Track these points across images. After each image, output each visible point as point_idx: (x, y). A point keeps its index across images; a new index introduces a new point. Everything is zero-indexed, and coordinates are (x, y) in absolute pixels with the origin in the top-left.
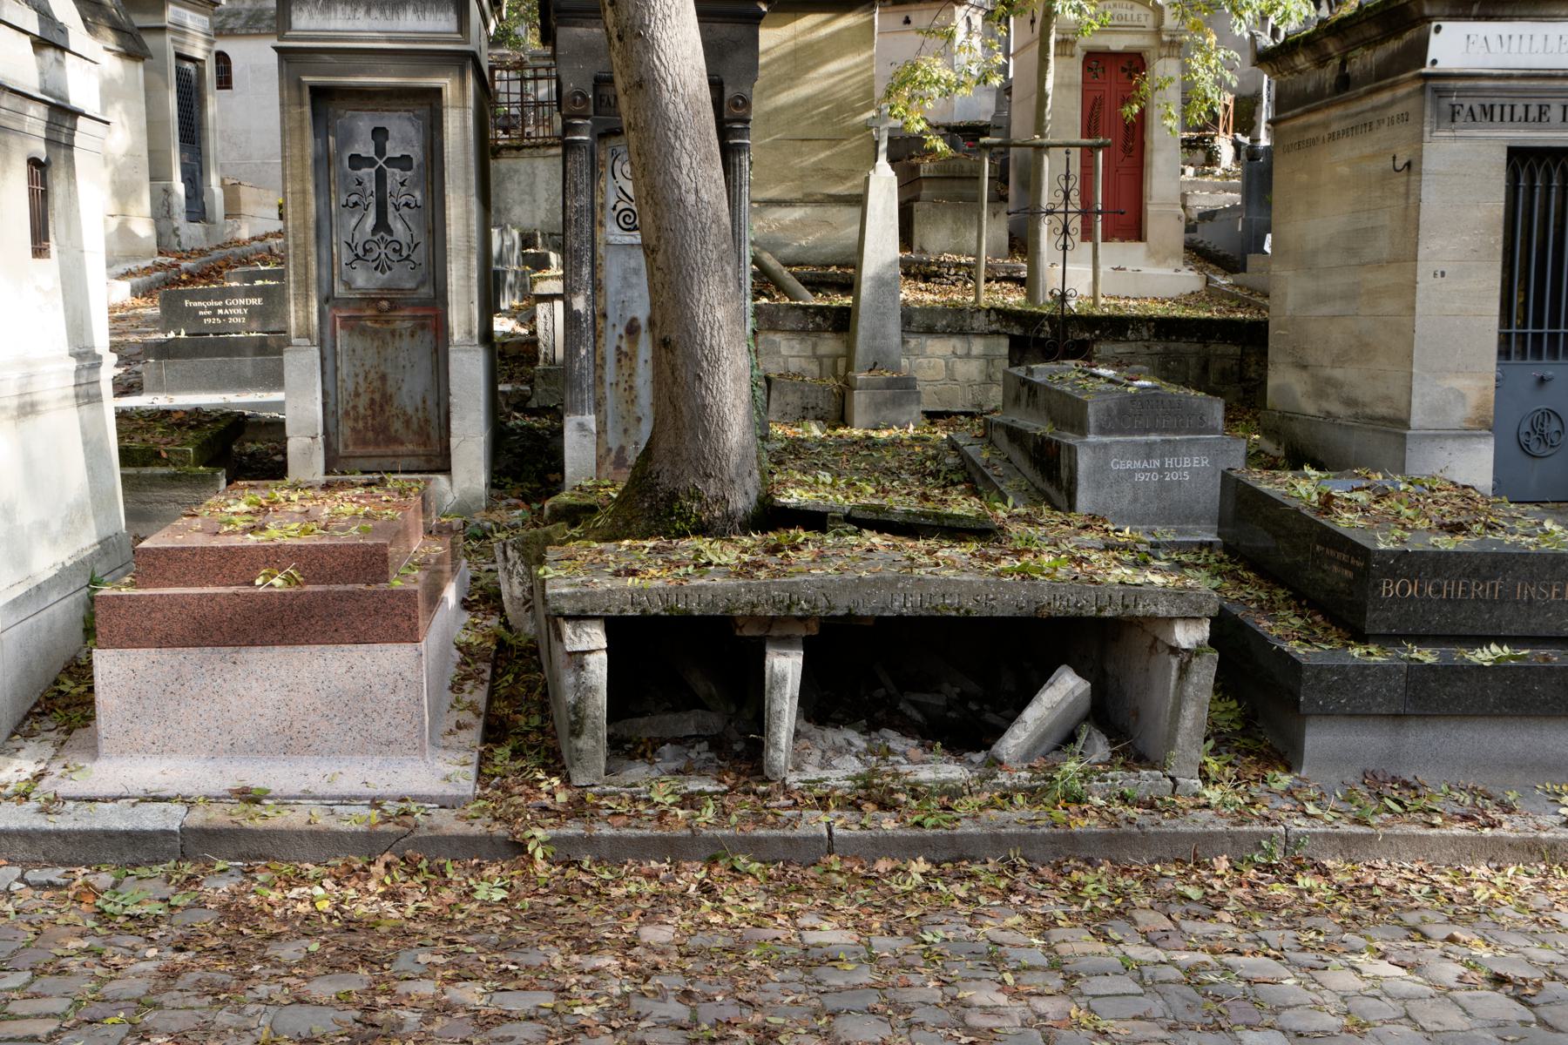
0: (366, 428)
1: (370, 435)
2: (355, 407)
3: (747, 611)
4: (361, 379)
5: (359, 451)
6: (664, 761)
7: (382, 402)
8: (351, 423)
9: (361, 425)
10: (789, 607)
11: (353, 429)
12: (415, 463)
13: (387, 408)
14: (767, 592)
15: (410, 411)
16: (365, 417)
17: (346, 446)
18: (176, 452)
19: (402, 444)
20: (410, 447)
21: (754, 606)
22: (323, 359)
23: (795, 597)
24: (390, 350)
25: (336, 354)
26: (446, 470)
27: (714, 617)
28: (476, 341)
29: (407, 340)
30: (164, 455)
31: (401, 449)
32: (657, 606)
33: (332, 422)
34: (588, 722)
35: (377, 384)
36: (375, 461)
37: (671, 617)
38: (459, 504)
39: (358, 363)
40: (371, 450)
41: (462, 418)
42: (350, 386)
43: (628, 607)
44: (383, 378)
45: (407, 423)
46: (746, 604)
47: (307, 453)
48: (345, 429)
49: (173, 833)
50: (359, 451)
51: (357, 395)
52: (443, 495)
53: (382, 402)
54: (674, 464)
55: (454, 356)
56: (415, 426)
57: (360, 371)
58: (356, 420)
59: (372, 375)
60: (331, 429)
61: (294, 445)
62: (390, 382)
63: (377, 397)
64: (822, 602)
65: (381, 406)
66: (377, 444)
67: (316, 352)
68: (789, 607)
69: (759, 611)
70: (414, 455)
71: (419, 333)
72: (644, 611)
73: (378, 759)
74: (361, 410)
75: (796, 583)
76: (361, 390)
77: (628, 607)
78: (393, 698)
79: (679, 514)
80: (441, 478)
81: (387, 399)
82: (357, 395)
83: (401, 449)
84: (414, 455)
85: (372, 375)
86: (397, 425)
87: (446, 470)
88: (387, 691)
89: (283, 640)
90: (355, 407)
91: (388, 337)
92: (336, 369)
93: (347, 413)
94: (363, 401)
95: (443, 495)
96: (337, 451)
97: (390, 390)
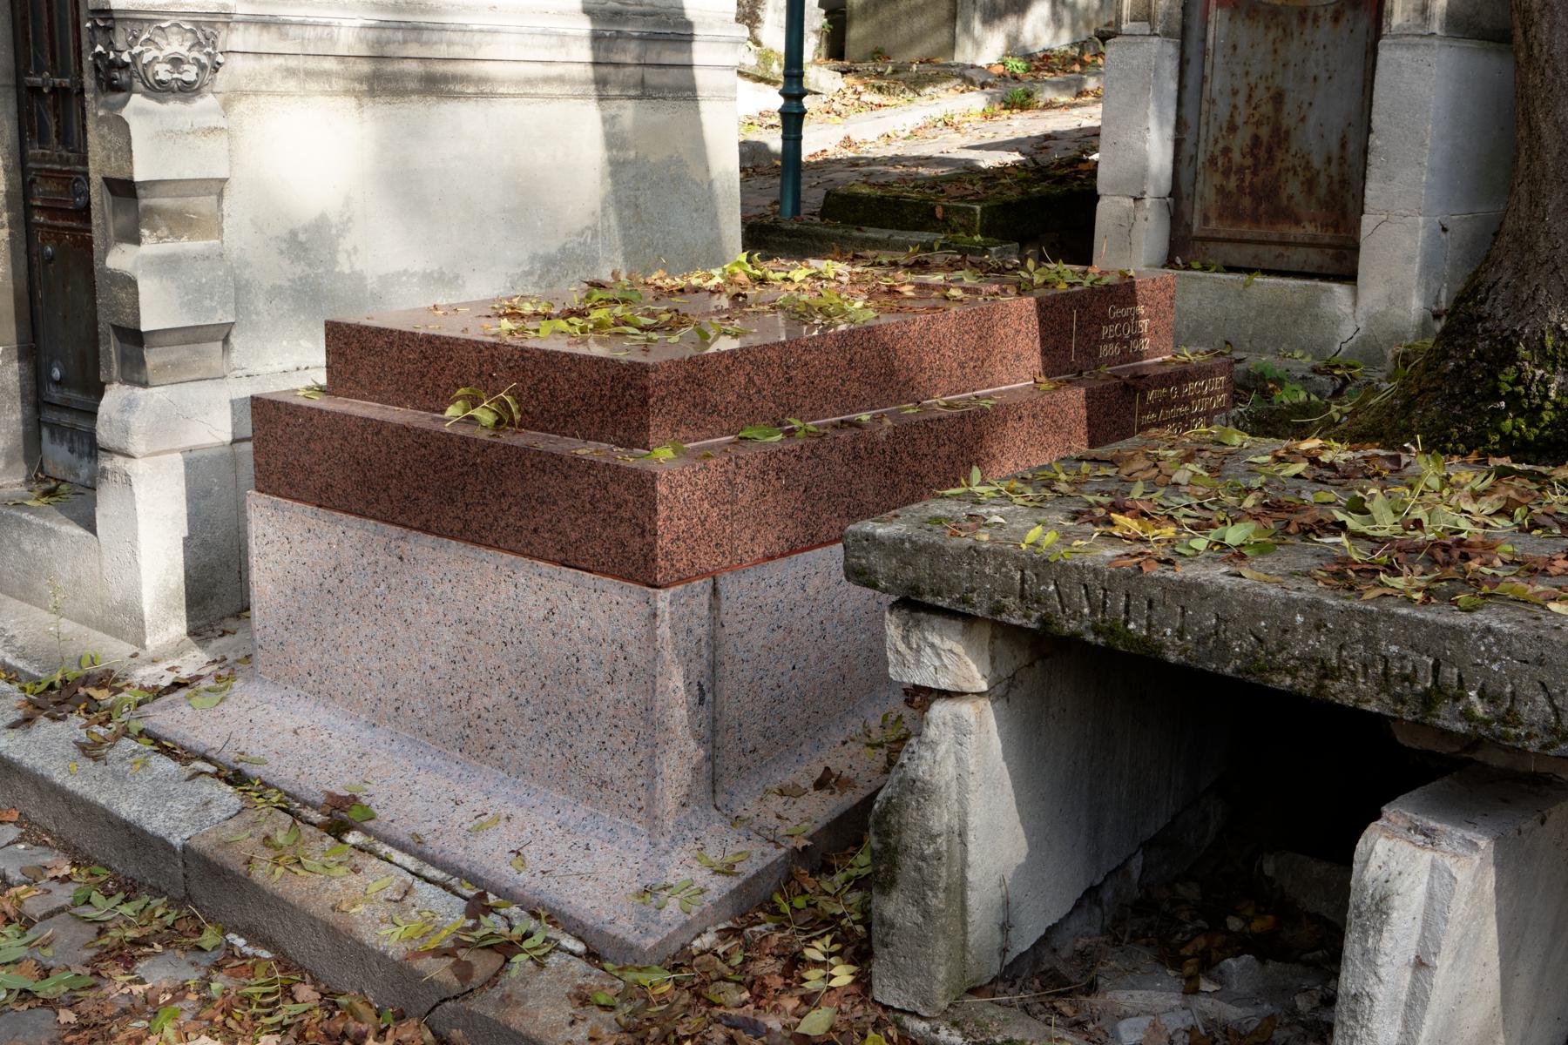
0: (1240, 188)
1: (1246, 202)
2: (1226, 151)
3: (1304, 683)
4: (1241, 100)
5: (1225, 230)
6: (1223, 995)
7: (1271, 144)
8: (1217, 179)
9: (1232, 183)
10: (1428, 701)
11: (1221, 190)
12: (1314, 258)
13: (1279, 155)
14: (1369, 641)
15: (1317, 162)
16: (1241, 170)
17: (1206, 219)
18: (958, 210)
19: (1298, 222)
20: (1310, 229)
21: (1327, 672)
22: (1183, 64)
23: (1450, 674)
24: (1295, 45)
25: (1204, 52)
26: (1348, 276)
27: (1216, 677)
28: (1436, 27)
29: (1326, 25)
30: (939, 212)
31: (1294, 232)
32: (1077, 615)
33: (1186, 175)
34: (907, 863)
35: (1267, 109)
36: (1250, 250)
37: (1108, 650)
38: (1363, 340)
39: (1239, 70)
40: (1246, 230)
41: (1389, 178)
42: (1222, 110)
43: (1011, 602)
44: (1278, 98)
45: (1310, 185)
46: (1307, 660)
47: (1127, 227)
48: (1206, 189)
49: (168, 847)
50: (1225, 230)
51: (1233, 128)
52: (1337, 322)
53: (1271, 144)
54: (1520, 272)
55: (1387, 54)
56: (1322, 191)
57: (1241, 84)
58: (1226, 174)
59: (1261, 93)
60: (1185, 188)
61: (1108, 210)
62: (1289, 106)
63: (1264, 132)
64: (1535, 710)
65: (1270, 151)
66: (1256, 220)
67: (1171, 49)
68: (1428, 701)
69: (1339, 690)
70: (1313, 244)
71: (1349, 14)
72: (1045, 621)
73: (583, 810)
74: (1236, 156)
75: (1457, 633)
76: (1239, 120)
77: (1011, 602)
78: (610, 694)
79: (1513, 398)
80: (1340, 290)
81: (1281, 137)
82: (1233, 128)
83: (1294, 232)
84: (1313, 244)
85: (1261, 93)
86: (1292, 187)
87: (1348, 276)
88: (601, 676)
89: (473, 532)
90: (1226, 151)
91: (1295, 21)
92: (1204, 79)
93: (1213, 161)
94: (1242, 139)
95: (1337, 322)
96: (1189, 226)
97: (1288, 122)
